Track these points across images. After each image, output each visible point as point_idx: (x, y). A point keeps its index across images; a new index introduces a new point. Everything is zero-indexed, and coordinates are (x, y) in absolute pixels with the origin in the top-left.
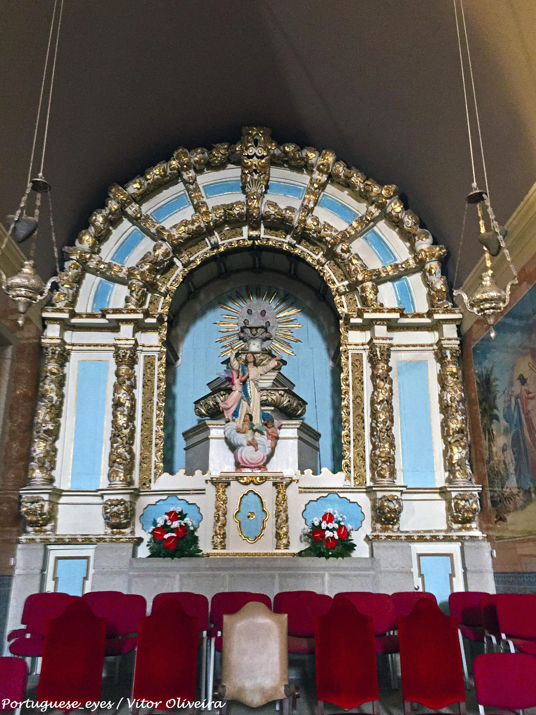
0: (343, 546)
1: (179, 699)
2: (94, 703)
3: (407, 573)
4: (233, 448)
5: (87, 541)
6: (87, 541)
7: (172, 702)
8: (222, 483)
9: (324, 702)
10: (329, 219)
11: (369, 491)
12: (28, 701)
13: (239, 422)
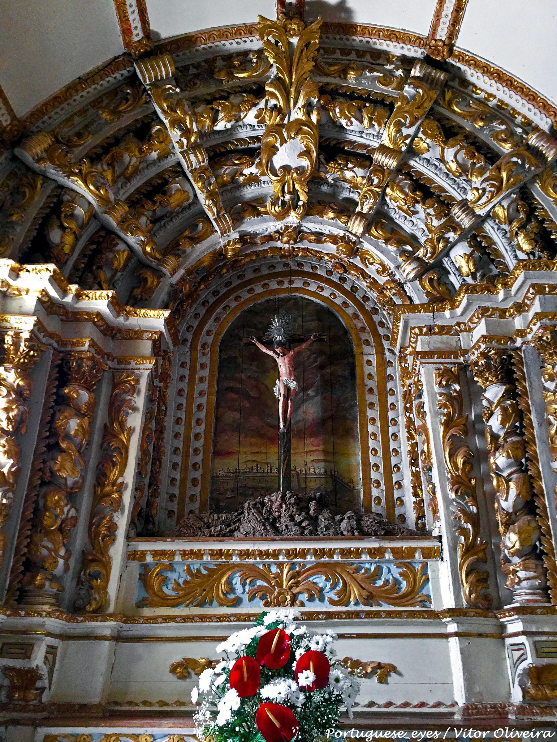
1: (507, 728)
2: (421, 733)
3: (30, 565)
9: (457, 623)
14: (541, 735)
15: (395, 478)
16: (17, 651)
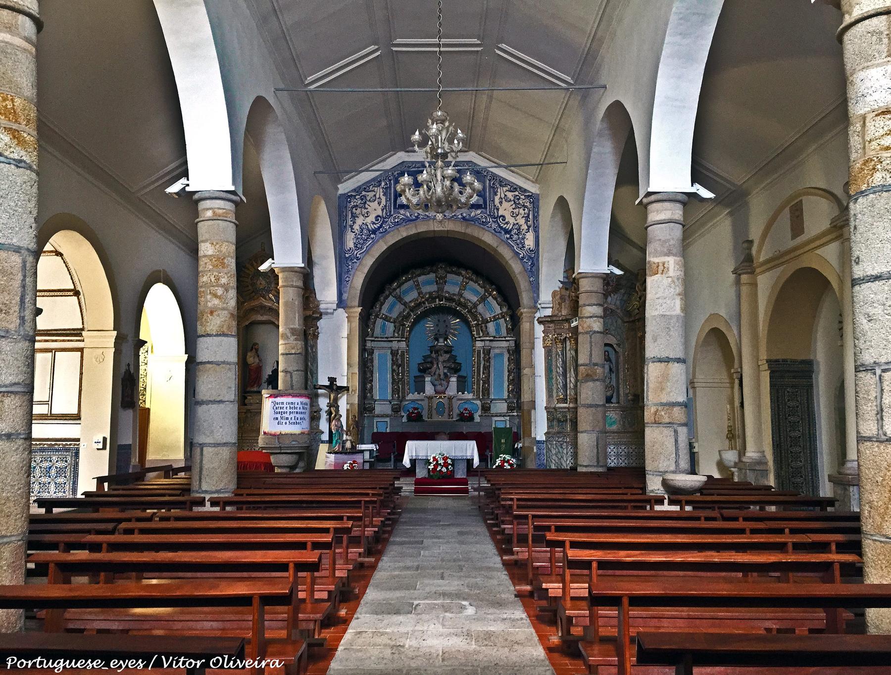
0: (471, 418)
1: (226, 657)
2: (121, 662)
4: (434, 385)
5: (387, 416)
6: (387, 416)
7: (218, 660)
8: (430, 398)
10: (472, 297)
11: (480, 400)
12: (39, 659)
13: (436, 377)
14: (268, 665)
15: (369, 386)
16: (233, 618)
